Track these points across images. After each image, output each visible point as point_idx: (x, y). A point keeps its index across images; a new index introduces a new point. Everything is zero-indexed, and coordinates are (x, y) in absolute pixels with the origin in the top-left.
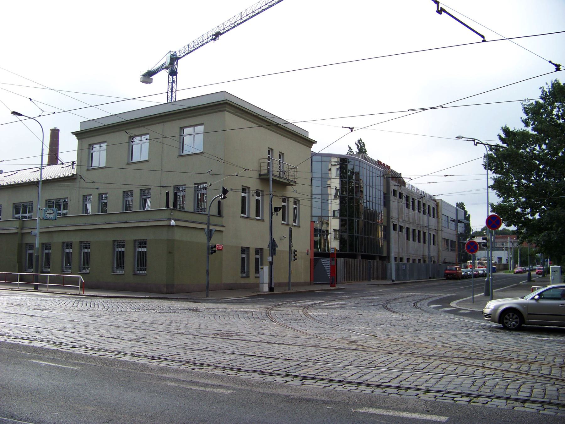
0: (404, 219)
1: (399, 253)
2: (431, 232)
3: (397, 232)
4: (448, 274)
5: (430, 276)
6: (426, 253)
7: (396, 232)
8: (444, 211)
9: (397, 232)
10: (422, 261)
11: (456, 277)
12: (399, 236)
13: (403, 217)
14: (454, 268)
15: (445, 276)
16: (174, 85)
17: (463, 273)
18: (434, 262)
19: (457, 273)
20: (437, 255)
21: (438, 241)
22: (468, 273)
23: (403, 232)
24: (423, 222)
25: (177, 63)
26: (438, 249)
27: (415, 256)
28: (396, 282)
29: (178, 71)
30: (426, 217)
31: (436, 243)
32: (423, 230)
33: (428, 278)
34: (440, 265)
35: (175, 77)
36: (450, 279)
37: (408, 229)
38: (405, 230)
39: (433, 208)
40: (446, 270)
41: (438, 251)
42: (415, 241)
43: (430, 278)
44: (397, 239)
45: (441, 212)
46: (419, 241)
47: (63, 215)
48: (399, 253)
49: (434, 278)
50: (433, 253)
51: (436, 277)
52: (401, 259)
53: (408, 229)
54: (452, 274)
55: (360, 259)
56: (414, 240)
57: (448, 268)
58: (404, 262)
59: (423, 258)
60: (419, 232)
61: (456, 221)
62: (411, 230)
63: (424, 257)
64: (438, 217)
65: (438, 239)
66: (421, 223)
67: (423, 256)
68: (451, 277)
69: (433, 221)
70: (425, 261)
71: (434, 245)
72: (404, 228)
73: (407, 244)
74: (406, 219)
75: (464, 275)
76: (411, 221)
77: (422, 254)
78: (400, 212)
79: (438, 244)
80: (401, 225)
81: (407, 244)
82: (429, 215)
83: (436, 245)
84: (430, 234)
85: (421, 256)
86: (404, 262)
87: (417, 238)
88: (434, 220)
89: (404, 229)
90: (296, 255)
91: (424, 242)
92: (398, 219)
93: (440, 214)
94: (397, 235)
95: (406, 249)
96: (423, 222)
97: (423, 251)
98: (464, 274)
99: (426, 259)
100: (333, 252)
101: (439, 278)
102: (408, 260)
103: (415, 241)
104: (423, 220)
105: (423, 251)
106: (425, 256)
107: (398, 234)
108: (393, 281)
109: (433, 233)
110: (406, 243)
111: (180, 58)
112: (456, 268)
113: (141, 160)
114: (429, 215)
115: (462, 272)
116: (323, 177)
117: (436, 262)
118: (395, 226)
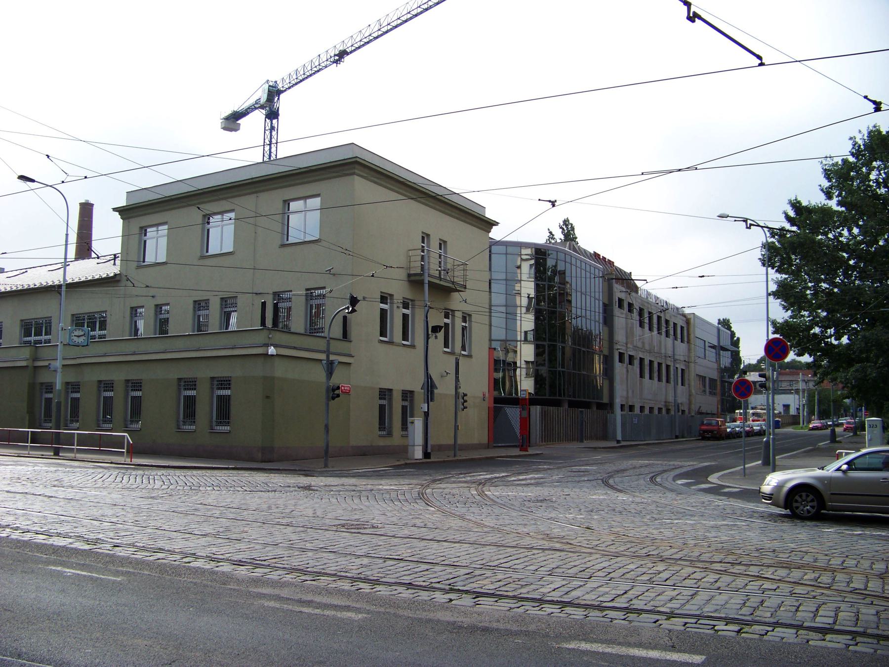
0: (635, 345)
1: (627, 398)
2: (677, 366)
3: (625, 365)
4: (705, 431)
5: (677, 434)
6: (671, 399)
7: (623, 366)
9: (625, 365)
10: (664, 411)
11: (718, 436)
12: (627, 371)
14: (714, 422)
15: (700, 435)
16: (274, 133)
17: (728, 430)
18: (683, 411)
19: (719, 429)
20: (688, 402)
21: (689, 380)
22: (737, 429)
23: (634, 365)
24: (666, 350)
25: (278, 99)
26: (690, 391)
27: (653, 402)
28: (623, 443)
29: (280, 112)
30: (670, 341)
31: (686, 382)
32: (665, 362)
33: (674, 437)
34: (693, 416)
35: (275, 121)
36: (708, 439)
37: (642, 360)
38: (636, 362)
39: (682, 328)
40: (703, 424)
41: (690, 395)
42: (653, 380)
43: (677, 437)
45: (694, 333)
46: (660, 380)
47: (99, 338)
48: (627, 398)
49: (683, 437)
50: (682, 399)
51: (686, 435)
52: (631, 408)
53: (642, 360)
54: (711, 431)
55: (567, 407)
56: (651, 378)
57: (705, 422)
58: (635, 413)
59: (666, 406)
60: (660, 364)
61: (717, 348)
62: (647, 362)
63: (668, 404)
64: (688, 342)
65: (689, 376)
66: (663, 351)
67: (666, 402)
68: (709, 435)
69: (681, 348)
70: (668, 411)
71: (682, 385)
72: (636, 358)
73: (641, 384)
74: (640, 345)
75: (730, 432)
76: (647, 347)
77: (664, 400)
78: (629, 334)
79: (689, 385)
80: (631, 353)
81: (641, 384)
83: (687, 386)
85: (663, 403)
86: (635, 413)
87: (656, 375)
88: (683, 346)
89: (635, 361)
91: (668, 381)
92: (627, 344)
93: (692, 336)
94: (625, 370)
95: (638, 392)
96: (666, 350)
97: (666, 395)
98: (730, 432)
99: (670, 408)
100: (525, 396)
101: (691, 437)
102: (642, 408)
103: (653, 380)
104: (665, 345)
105: (666, 395)
106: (669, 402)
107: (627, 368)
108: (618, 442)
109: (681, 366)
110: (638, 382)
111: (283, 92)
112: (718, 421)
113: (222, 252)
114: (676, 339)
115: (726, 428)
116: (508, 278)
117: (687, 412)
118: (621, 355)
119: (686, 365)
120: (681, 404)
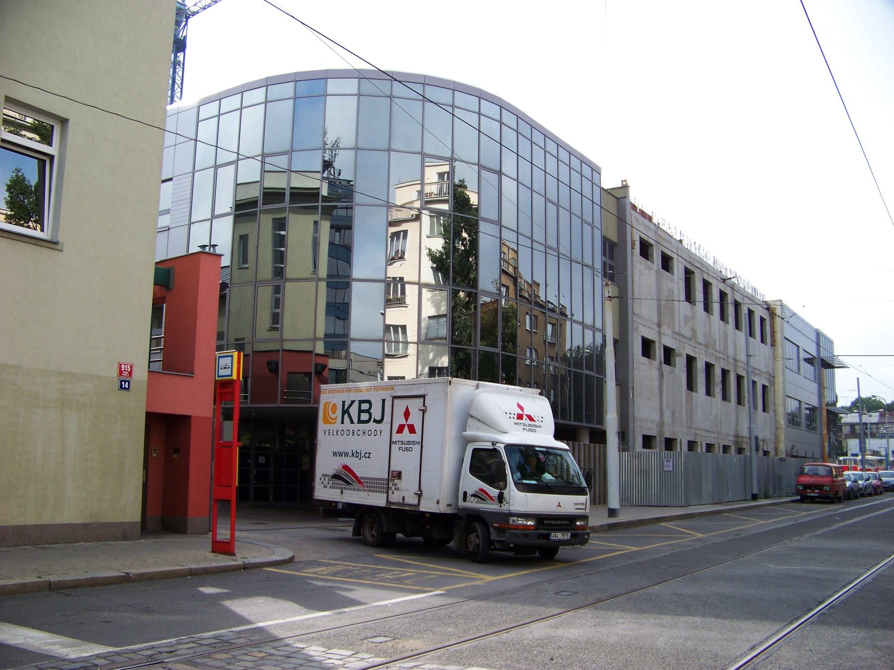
0: (677, 330)
1: (661, 424)
2: (756, 379)
3: (656, 363)
4: (807, 486)
5: (755, 492)
6: (745, 432)
7: (650, 364)
8: (784, 330)
9: (656, 363)
10: (733, 450)
11: (831, 495)
12: (661, 376)
13: (677, 324)
14: (821, 471)
15: (798, 492)
16: (179, 71)
17: (848, 484)
18: (766, 453)
19: (833, 482)
20: (773, 438)
21: (774, 403)
22: (860, 482)
23: (675, 366)
24: (735, 349)
25: (186, 24)
26: (776, 421)
27: (712, 435)
28: (622, 518)
29: (188, 43)
30: (742, 336)
31: (771, 407)
32: (735, 370)
33: (749, 497)
34: (781, 459)
35: (180, 56)
36: (813, 500)
37: (690, 360)
38: (680, 362)
39: (762, 320)
40: (802, 473)
41: (777, 429)
42: (714, 396)
43: (755, 497)
44: (656, 383)
45: (782, 331)
46: (725, 397)
47: (284, 401)
48: (661, 424)
49: (766, 497)
50: (764, 433)
51: (771, 492)
52: (670, 444)
53: (690, 360)
54: (819, 487)
55: (587, 443)
56: (709, 393)
57: (807, 469)
58: (385, 381)
59: (736, 443)
60: (725, 373)
61: (816, 362)
62: (700, 366)
63: (740, 440)
64: (773, 344)
65: (774, 398)
66: (731, 351)
67: (736, 436)
68: (815, 493)
69: (760, 350)
70: (740, 451)
71: (764, 410)
72: (680, 355)
73: (689, 401)
74: (687, 332)
75: (851, 488)
76: (701, 338)
77: (734, 433)
78: (663, 306)
79: (775, 411)
80: (670, 344)
81: (689, 401)
82: (751, 334)
83: (771, 413)
84: (754, 382)
85: (731, 438)
86: (385, 381)
87: (718, 389)
88: (765, 349)
89: (677, 358)
90: (329, 432)
91: (739, 402)
92: (659, 326)
93: (778, 336)
94: (655, 374)
95: (684, 417)
96: (735, 349)
98: (850, 486)
99: (745, 446)
100: (228, 372)
101: (780, 497)
102: (692, 445)
103: (714, 396)
104: (735, 344)
105: (737, 423)
106: (742, 437)
107: (660, 369)
108: (612, 513)
109: (761, 381)
110: (684, 400)
112: (831, 467)
113: (168, 258)
114: (751, 334)
115: (844, 481)
116: (359, 145)
117: (772, 453)
118: (647, 346)
119: (770, 381)
120: (763, 441)
